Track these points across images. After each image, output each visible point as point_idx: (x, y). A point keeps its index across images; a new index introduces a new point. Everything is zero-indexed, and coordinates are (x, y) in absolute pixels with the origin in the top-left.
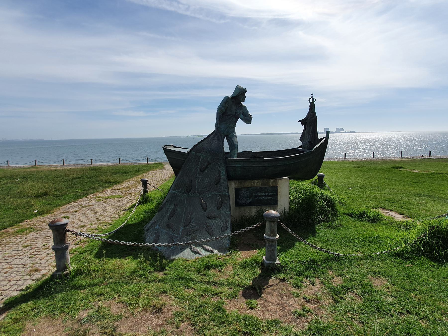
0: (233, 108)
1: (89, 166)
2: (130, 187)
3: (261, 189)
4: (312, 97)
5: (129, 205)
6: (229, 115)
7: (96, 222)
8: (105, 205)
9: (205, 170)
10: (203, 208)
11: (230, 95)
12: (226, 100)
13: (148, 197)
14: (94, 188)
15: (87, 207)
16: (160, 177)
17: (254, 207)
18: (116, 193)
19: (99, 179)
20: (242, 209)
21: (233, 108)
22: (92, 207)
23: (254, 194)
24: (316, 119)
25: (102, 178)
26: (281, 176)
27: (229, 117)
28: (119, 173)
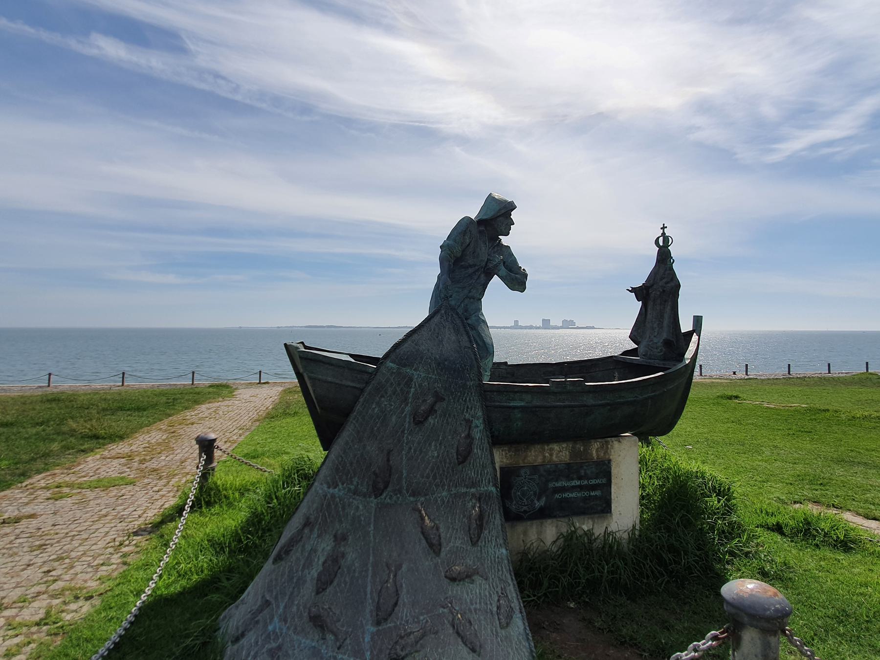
0: (479, 251)
1: (39, 392)
2: (151, 451)
3: (568, 471)
4: (663, 234)
5: (152, 514)
6: (471, 266)
7: (42, 588)
8: (78, 514)
9: (426, 418)
10: (431, 545)
11: (473, 213)
12: (464, 228)
13: (217, 487)
14: (46, 455)
15: (17, 520)
16: (230, 420)
17: (549, 521)
18: (113, 469)
19: (65, 429)
20: (520, 528)
21: (479, 251)
22: (34, 523)
23: (551, 485)
24: (679, 286)
25: (74, 425)
26: (613, 432)
27: (470, 271)
28: (121, 409)
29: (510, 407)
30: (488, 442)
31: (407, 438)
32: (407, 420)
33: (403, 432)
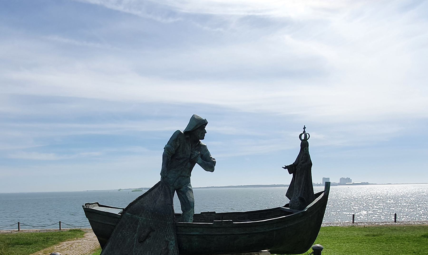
0: (187, 149)
4: (304, 132)
6: (182, 159)
9: (145, 240)
11: (182, 129)
12: (177, 137)
16: (79, 250)
21: (187, 149)
24: (311, 164)
27: (181, 161)
28: (18, 244)
29: (191, 235)
30: (177, 252)
31: (135, 249)
32: (135, 241)
33: (133, 246)
